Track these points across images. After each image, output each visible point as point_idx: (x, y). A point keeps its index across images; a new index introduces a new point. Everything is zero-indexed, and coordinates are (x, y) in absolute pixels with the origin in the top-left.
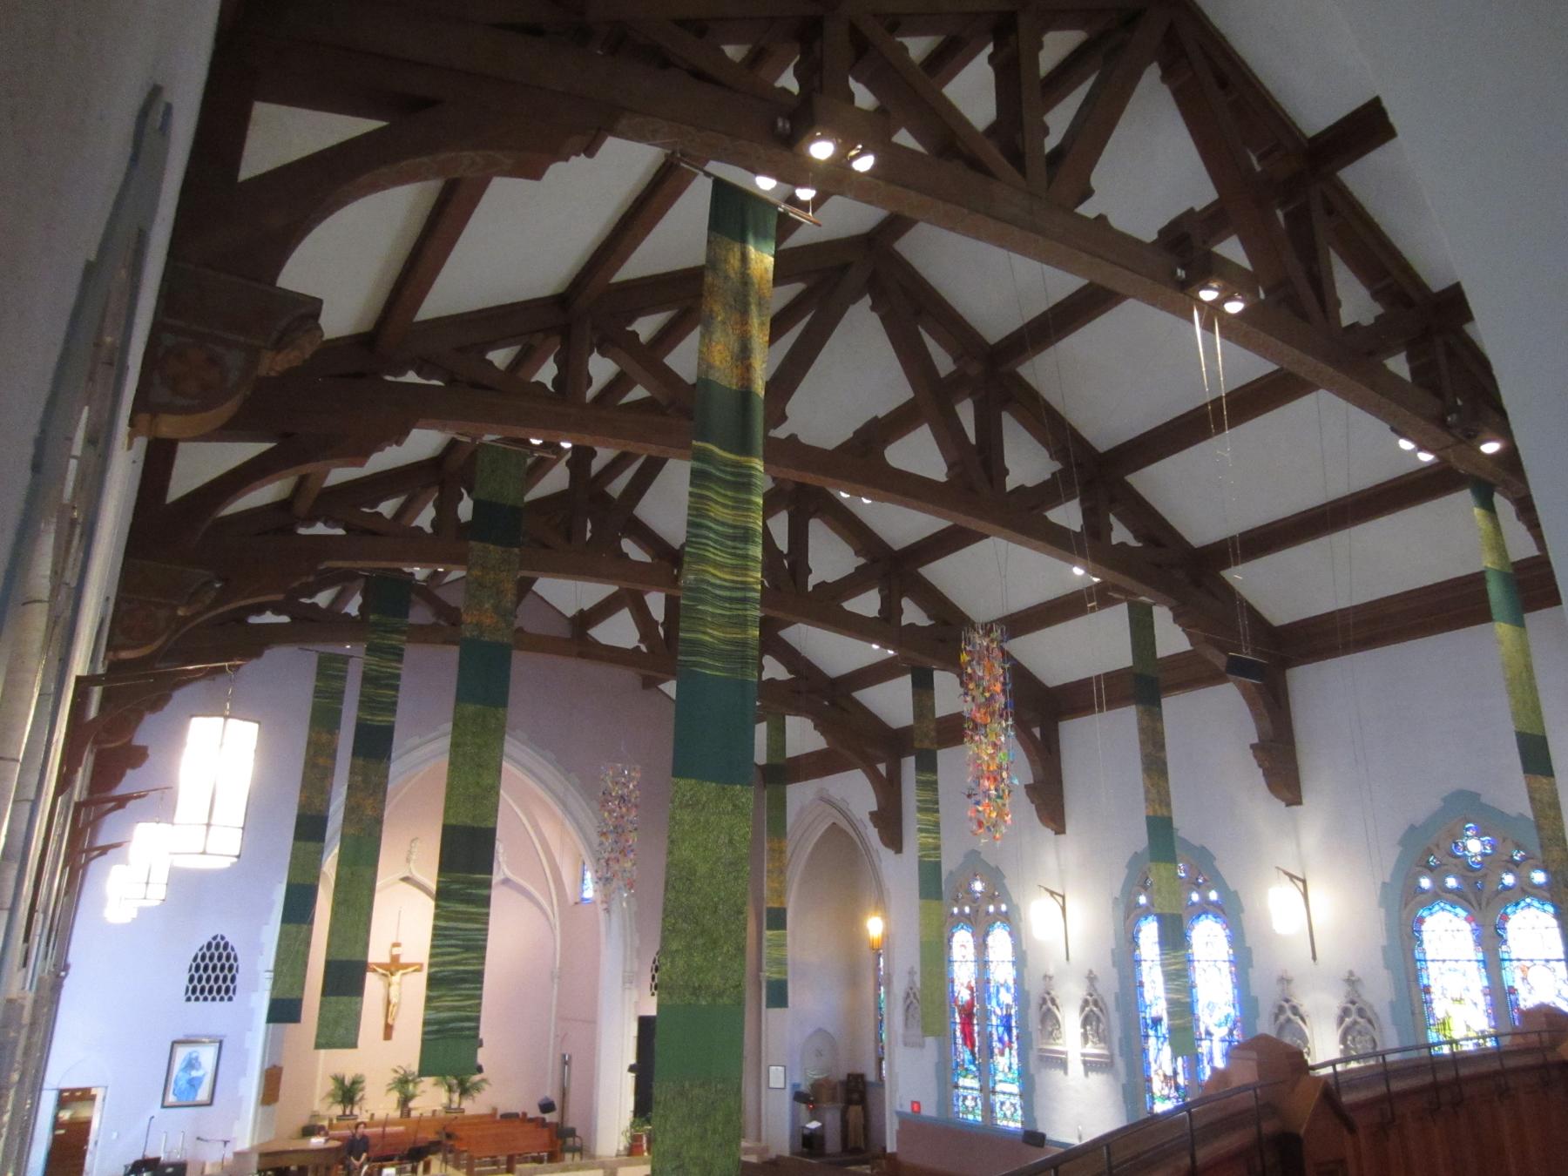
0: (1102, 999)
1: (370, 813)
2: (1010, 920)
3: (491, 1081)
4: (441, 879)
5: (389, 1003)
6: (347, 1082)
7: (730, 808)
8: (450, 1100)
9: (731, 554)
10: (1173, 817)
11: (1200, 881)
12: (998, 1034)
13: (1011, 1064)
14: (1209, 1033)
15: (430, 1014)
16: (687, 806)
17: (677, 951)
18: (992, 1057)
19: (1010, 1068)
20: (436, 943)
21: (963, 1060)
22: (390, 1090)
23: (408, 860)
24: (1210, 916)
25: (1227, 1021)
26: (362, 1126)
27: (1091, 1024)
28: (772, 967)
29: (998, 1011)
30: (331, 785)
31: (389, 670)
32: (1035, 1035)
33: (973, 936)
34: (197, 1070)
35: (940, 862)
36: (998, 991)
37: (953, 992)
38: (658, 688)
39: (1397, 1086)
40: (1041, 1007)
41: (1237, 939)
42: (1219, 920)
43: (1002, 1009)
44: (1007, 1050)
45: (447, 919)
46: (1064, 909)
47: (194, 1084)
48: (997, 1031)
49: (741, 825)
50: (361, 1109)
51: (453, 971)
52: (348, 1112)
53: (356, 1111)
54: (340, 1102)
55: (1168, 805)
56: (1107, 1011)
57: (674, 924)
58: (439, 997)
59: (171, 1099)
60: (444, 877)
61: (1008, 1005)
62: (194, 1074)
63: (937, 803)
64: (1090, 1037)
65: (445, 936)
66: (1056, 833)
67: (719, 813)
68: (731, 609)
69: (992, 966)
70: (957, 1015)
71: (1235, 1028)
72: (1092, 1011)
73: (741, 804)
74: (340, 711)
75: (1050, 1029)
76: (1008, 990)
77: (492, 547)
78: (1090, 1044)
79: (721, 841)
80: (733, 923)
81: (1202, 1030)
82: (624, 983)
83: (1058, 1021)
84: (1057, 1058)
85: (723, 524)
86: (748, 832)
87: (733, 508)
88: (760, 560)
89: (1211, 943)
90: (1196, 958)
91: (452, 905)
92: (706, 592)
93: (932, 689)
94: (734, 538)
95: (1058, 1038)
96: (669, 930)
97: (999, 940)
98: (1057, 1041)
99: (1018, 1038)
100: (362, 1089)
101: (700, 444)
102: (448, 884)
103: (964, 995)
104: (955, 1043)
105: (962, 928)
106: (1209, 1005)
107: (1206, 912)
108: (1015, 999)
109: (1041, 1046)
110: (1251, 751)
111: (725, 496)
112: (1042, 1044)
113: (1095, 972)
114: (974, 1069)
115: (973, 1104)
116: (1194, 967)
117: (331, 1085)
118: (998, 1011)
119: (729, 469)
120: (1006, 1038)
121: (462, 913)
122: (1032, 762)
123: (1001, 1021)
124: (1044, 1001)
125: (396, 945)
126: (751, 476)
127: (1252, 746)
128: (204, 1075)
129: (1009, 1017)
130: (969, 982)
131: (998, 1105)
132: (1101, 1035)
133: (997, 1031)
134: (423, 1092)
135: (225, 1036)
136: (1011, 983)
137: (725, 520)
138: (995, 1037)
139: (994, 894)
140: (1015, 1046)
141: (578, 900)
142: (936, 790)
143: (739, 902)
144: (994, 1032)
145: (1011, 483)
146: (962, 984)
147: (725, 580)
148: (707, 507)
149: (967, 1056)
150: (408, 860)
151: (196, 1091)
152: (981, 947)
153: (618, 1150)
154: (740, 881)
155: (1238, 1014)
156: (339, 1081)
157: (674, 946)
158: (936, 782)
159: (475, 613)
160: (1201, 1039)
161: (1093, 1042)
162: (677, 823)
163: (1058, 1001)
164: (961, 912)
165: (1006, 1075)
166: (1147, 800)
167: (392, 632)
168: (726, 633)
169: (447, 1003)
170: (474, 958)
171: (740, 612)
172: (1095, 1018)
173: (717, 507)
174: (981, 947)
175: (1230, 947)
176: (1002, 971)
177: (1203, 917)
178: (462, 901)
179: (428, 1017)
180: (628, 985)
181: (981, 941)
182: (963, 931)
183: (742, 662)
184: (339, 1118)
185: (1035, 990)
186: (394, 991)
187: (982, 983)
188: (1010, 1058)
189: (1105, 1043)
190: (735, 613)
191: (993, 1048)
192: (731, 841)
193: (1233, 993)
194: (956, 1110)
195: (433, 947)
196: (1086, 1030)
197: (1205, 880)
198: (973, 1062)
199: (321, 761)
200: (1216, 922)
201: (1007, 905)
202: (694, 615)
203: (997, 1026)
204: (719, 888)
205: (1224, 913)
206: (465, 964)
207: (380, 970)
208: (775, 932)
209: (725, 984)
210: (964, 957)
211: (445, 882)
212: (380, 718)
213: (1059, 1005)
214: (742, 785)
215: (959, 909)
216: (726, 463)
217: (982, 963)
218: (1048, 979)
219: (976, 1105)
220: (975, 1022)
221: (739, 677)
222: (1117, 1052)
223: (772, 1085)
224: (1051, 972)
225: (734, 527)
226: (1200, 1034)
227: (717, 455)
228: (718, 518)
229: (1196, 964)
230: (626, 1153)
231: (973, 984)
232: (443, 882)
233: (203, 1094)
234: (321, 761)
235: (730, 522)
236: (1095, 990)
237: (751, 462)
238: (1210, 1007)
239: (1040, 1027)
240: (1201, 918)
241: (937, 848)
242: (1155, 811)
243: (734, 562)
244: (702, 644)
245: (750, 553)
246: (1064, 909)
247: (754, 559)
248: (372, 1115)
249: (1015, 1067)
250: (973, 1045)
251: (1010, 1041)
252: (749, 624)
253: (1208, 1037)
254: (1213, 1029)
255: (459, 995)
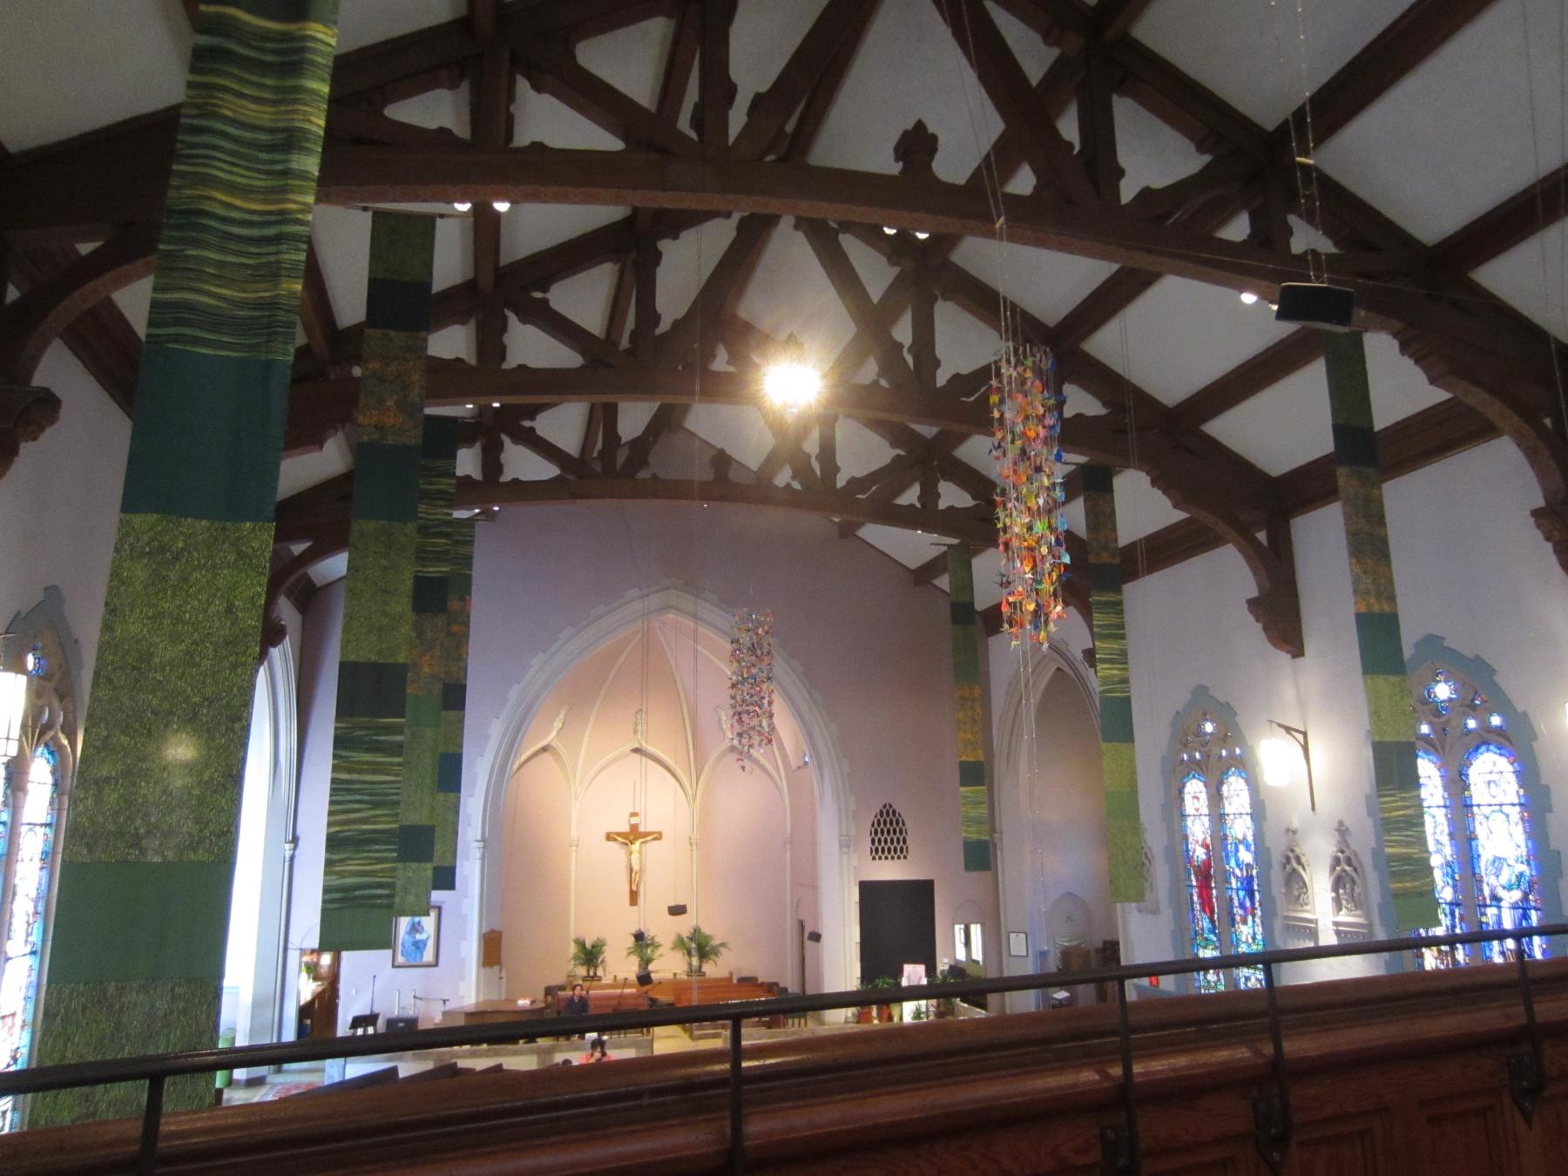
0: (1356, 855)
1: (428, 670)
2: (1244, 765)
3: (730, 946)
4: (339, 725)
5: (631, 870)
6: (588, 945)
7: (232, 557)
8: (690, 964)
9: (268, 173)
10: (1400, 613)
11: (1477, 702)
12: (1239, 899)
13: (1255, 934)
14: (1496, 899)
15: (331, 880)
16: (142, 555)
17: (107, 780)
18: (1234, 926)
19: (1254, 938)
20: (333, 798)
21: (1202, 929)
22: (630, 954)
23: (635, 732)
24: (1492, 747)
25: (1519, 882)
26: (579, 988)
27: (1345, 888)
28: (969, 826)
29: (1238, 872)
30: (467, 653)
31: (438, 517)
32: (1280, 902)
33: (1206, 786)
34: (421, 933)
35: (1129, 698)
36: (1237, 850)
37: (1188, 851)
38: (854, 535)
39: (1299, 1046)
40: (1285, 867)
41: (1528, 774)
42: (1503, 751)
43: (1241, 870)
44: (1250, 918)
45: (350, 771)
46: (1305, 748)
47: (419, 946)
48: (1238, 896)
49: (249, 582)
50: (604, 970)
51: (358, 830)
52: (591, 973)
53: (600, 972)
54: (583, 965)
55: (1392, 598)
56: (1363, 872)
57: (107, 737)
58: (341, 861)
59: (400, 959)
60: (342, 722)
61: (1248, 865)
62: (418, 937)
63: (1122, 627)
64: (1344, 902)
65: (347, 790)
66: (1294, 656)
67: (214, 566)
68: (257, 254)
69: (1229, 820)
70: (1193, 877)
71: (1531, 891)
72: (1345, 871)
73: (250, 551)
74: (470, 576)
75: (1296, 893)
76: (1248, 848)
77: (392, 334)
78: (1344, 911)
79: (212, 609)
80: (223, 735)
81: (1487, 892)
82: (841, 847)
83: (1304, 883)
84: (1305, 927)
85: (253, 128)
86: (259, 595)
87: (274, 103)
88: (316, 178)
89: (1494, 782)
90: (1475, 802)
91: (354, 754)
92: (207, 228)
93: (1112, 491)
94: (272, 148)
95: (1306, 904)
96: (95, 747)
97: (1236, 793)
98: (1306, 908)
99: (1260, 905)
100: (602, 953)
101: (212, 9)
102: (349, 731)
103: (1200, 854)
104: (1193, 910)
105: (1194, 777)
106: (1494, 862)
107: (1487, 743)
108: (1256, 859)
109: (1286, 914)
110: (1533, 520)
111: (262, 86)
112: (1288, 910)
113: (1347, 823)
114: (1215, 939)
115: (1215, 978)
116: (1473, 814)
117: (573, 949)
118: (1238, 872)
119: (270, 45)
120: (1248, 904)
121: (367, 763)
122: (1255, 571)
123: (1242, 884)
124: (1288, 860)
125: (634, 814)
126: (303, 50)
127: (1536, 513)
128: (428, 938)
129: (1250, 879)
130: (1205, 839)
131: (1243, 980)
132: (1357, 900)
133: (1238, 896)
134: (660, 956)
135: (443, 902)
136: (1250, 839)
137: (258, 122)
138: (1236, 903)
139: (1226, 735)
140: (1259, 912)
141: (801, 764)
142: (1121, 612)
143: (236, 702)
144: (1234, 896)
145: (1128, 191)
146: (1197, 842)
147: (254, 212)
148: (216, 101)
149: (1206, 924)
150: (635, 732)
151: (422, 954)
152: (1216, 798)
153: (846, 1017)
154: (239, 670)
155: (1534, 873)
156: (581, 944)
157: (104, 771)
158: (1120, 603)
159: (373, 412)
160: (1486, 906)
161: (1347, 908)
162: (124, 583)
163: (1303, 860)
164: (1192, 758)
165: (1249, 946)
166: (1355, 592)
167: (439, 476)
168: (244, 292)
169: (353, 868)
170: (385, 815)
171: (272, 259)
172: (1348, 880)
173: (244, 102)
174: (1216, 798)
175: (1521, 787)
176: (1241, 827)
177: (1483, 748)
178: (367, 750)
179: (329, 883)
180: (845, 850)
181: (1214, 791)
182: (1195, 781)
183: (268, 334)
184: (584, 979)
185: (1277, 848)
186: (635, 858)
187: (1219, 839)
188: (1253, 927)
189: (1361, 908)
190: (263, 260)
191: (1234, 915)
192: (229, 610)
193: (1527, 847)
194: (1197, 985)
195: (331, 803)
196: (1337, 893)
197: (1483, 701)
198: (1212, 931)
199: (455, 628)
200: (1501, 755)
201: (1241, 749)
202: (180, 265)
203: (1238, 890)
204: (203, 683)
205: (1511, 743)
206: (374, 823)
207: (620, 839)
208: (968, 788)
209: (201, 831)
210: (1197, 810)
211: (346, 728)
212: (431, 569)
213: (1305, 864)
214: (254, 520)
215: (1188, 755)
216: (265, 36)
217: (1218, 818)
218: (1291, 834)
219: (1219, 980)
220: (1213, 885)
221: (263, 357)
222: (1377, 921)
223: (1013, 953)
224: (1295, 824)
225: (272, 131)
226: (1484, 899)
227: (249, 24)
228: (242, 118)
229: (1475, 809)
230: (855, 1020)
231: (1208, 841)
232: (341, 728)
233: (428, 956)
234: (455, 628)
235: (268, 124)
236: (1348, 846)
237: (305, 30)
238: (1496, 865)
239: (1283, 890)
240: (1480, 751)
241: (1125, 681)
242: (1369, 605)
243: (269, 183)
244: (190, 307)
245: (294, 166)
246: (1305, 748)
247: (304, 175)
248: (615, 977)
249: (1259, 937)
250: (1212, 912)
251: (1253, 908)
252: (284, 272)
253: (1494, 903)
254: (1502, 893)
255: (371, 858)
